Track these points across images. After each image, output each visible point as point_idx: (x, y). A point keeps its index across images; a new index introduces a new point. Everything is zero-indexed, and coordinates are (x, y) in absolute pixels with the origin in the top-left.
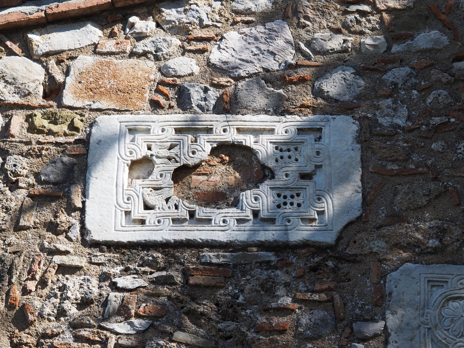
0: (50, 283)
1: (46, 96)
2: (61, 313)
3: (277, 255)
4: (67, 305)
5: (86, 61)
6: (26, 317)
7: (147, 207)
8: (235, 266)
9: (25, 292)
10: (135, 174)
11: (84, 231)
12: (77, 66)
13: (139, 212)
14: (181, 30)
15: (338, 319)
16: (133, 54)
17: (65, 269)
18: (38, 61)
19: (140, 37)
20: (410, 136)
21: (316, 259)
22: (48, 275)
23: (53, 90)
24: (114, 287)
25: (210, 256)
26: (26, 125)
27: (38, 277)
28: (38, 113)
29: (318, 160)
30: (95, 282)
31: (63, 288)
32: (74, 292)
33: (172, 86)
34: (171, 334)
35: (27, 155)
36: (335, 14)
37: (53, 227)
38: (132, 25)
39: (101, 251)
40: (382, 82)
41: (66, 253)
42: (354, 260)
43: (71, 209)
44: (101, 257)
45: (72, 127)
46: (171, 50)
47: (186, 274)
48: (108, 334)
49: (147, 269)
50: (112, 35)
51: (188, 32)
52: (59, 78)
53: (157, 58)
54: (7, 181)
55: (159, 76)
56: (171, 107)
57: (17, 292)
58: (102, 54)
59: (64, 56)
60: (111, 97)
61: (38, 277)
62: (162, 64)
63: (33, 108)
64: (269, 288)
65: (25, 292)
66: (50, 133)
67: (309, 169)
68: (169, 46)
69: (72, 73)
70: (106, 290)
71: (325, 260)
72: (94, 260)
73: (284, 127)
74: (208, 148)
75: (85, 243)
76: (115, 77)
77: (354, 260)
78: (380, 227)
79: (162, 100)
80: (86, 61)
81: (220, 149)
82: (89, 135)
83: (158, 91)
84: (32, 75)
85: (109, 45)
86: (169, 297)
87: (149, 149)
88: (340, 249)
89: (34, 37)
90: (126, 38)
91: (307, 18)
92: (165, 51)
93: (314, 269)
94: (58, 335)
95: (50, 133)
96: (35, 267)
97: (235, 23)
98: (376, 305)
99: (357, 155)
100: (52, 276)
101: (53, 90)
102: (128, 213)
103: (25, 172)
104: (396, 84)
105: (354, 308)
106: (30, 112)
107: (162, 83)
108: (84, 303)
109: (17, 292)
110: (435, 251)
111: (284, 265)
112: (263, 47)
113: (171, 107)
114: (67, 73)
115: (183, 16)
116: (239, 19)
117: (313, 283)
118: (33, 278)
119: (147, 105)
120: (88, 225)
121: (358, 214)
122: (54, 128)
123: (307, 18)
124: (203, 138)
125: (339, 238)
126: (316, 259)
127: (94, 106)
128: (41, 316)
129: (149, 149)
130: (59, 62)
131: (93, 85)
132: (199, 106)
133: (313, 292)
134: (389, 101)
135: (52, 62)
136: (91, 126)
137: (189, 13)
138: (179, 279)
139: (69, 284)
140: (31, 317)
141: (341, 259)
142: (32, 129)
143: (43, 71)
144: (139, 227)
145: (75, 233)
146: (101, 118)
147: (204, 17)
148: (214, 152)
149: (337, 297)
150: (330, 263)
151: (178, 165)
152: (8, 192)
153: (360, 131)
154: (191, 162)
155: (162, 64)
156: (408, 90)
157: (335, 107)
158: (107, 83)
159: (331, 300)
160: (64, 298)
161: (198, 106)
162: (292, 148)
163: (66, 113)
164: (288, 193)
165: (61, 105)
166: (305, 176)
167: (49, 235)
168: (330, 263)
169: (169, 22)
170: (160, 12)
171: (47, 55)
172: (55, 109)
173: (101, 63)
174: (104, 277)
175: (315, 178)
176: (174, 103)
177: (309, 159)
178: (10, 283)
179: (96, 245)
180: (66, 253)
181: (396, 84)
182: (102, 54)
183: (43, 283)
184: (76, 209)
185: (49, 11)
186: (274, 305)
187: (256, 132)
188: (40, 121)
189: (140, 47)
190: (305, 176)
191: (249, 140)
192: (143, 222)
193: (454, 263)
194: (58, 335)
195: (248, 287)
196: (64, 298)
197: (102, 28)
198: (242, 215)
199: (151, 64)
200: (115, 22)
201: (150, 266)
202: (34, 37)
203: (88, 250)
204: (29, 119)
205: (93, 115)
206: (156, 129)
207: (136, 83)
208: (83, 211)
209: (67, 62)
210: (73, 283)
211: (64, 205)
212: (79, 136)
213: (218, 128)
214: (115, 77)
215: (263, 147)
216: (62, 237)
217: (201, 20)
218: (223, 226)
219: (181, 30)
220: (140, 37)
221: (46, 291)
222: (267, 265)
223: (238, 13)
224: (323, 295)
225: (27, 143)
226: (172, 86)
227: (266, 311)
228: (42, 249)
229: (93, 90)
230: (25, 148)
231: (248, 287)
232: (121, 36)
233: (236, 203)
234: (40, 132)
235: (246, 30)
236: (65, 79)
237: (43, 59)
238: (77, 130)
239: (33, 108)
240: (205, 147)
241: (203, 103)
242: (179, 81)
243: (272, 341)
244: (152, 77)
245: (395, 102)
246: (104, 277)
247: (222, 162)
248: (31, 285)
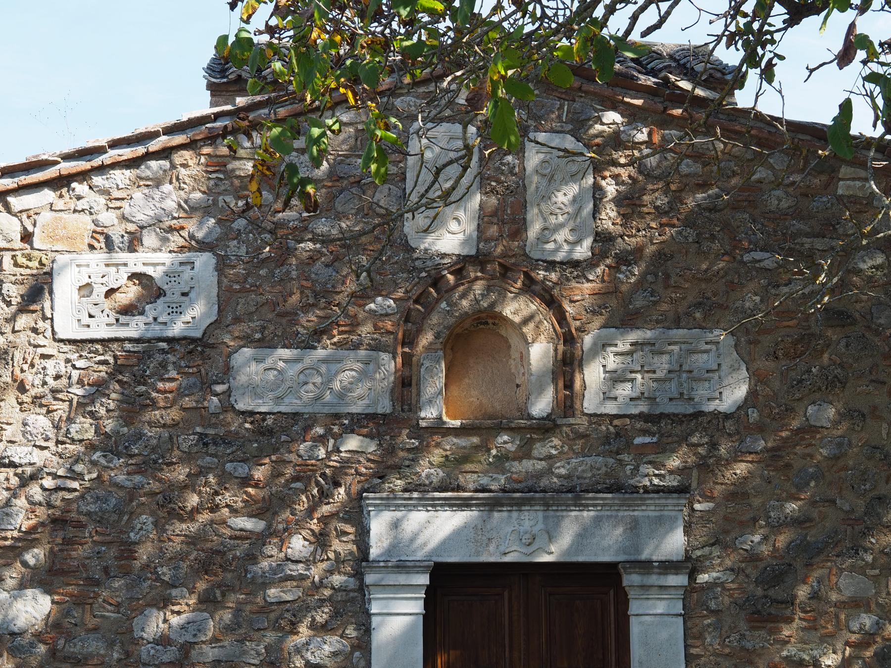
0: (36, 366)
1: (22, 239)
2: (45, 383)
3: (168, 345)
4: (48, 379)
5: (46, 217)
6: (24, 387)
7: (91, 316)
8: (144, 352)
9: (22, 371)
10: (82, 293)
11: (54, 332)
12: (40, 219)
13: (86, 320)
14: (105, 192)
15: (203, 383)
16: (75, 211)
17: (44, 357)
18: (15, 215)
19: (79, 198)
20: (248, 266)
21: (191, 347)
22: (34, 361)
23: (27, 237)
24: (74, 367)
25: (128, 346)
26: (12, 262)
27: (29, 362)
28: (18, 253)
29: (192, 284)
30: (63, 364)
31: (44, 368)
32: (51, 371)
33: (102, 233)
34: (109, 395)
35: (14, 283)
36: (203, 180)
37: (35, 330)
38: (74, 190)
39: (65, 344)
40: (231, 228)
41: (44, 346)
42: (212, 346)
43: (44, 318)
44: (66, 348)
45: (41, 263)
46: (99, 208)
47: (115, 357)
48: (73, 396)
49: (92, 355)
50: (61, 196)
51: (109, 194)
52: (30, 228)
53: (91, 214)
54: (4, 300)
55: (93, 227)
56: (101, 248)
57: (17, 371)
58: (56, 211)
59: (32, 212)
60: (562, 516)
61: (29, 362)
62: (94, 217)
63: (16, 250)
64: (163, 365)
65: (22, 371)
66: (27, 267)
67: (186, 290)
68: (98, 205)
69: (37, 225)
70: (70, 368)
71: (196, 346)
72: (61, 350)
73: (165, 258)
74: (126, 277)
75: (55, 340)
76: (65, 228)
77: (212, 346)
78: (227, 326)
79: (96, 244)
80: (46, 217)
81: (133, 276)
82: (52, 268)
83: (92, 237)
84: (13, 227)
85: (60, 204)
86: (107, 373)
87: (90, 277)
88: (205, 340)
89: (10, 199)
90: (71, 198)
91: (185, 183)
92: (96, 208)
93: (190, 352)
94: (44, 397)
95: (27, 267)
96: (27, 356)
97: (139, 186)
98: (225, 374)
99: (215, 280)
100: (37, 361)
101: (27, 237)
102: (79, 320)
103: (14, 295)
104: (240, 230)
105: (212, 376)
106: (14, 253)
107: (94, 232)
108: (57, 377)
109: (17, 371)
110: (259, 340)
111: (172, 351)
112: (158, 205)
113: (101, 248)
114: (35, 225)
115: (106, 182)
116: (142, 183)
117: (189, 361)
118: (26, 363)
119: (86, 247)
120: (56, 329)
121: (215, 318)
122: (30, 264)
123: (185, 183)
124: (122, 268)
125: (204, 334)
126: (191, 347)
127: (54, 249)
128: (33, 385)
129: (90, 277)
130: (29, 217)
131: (52, 234)
132: (119, 247)
133: (189, 367)
134: (235, 242)
135: (24, 216)
136: (53, 262)
137: (110, 180)
138: (112, 361)
139: (47, 366)
140: (27, 387)
141: (207, 346)
142: (16, 265)
143: (20, 224)
144: (86, 329)
145: (49, 334)
146: (59, 257)
147: (119, 183)
148: (129, 278)
149: (203, 370)
150: (199, 349)
151: (108, 288)
152: (6, 308)
153: (217, 263)
154: (115, 287)
155: (94, 217)
156: (247, 234)
157: (203, 246)
158: (61, 232)
159: (200, 371)
160: (45, 375)
161: (119, 247)
162: (176, 275)
163: (36, 253)
164: (174, 305)
165: (32, 248)
166: (184, 294)
167: (33, 335)
168: (199, 349)
169: (97, 186)
170: (91, 179)
171: (21, 212)
172: (29, 251)
173: (56, 218)
174: (68, 361)
175: (191, 295)
176: (103, 245)
177: (187, 283)
178: (13, 366)
179: (61, 341)
180: (44, 346)
181: (240, 230)
182: (56, 211)
183: (32, 365)
184: (48, 319)
185: (20, 183)
186: (166, 376)
187: (155, 265)
188: (21, 260)
189: (81, 205)
190: (184, 294)
191: (149, 271)
192: (88, 326)
193: (270, 348)
194: (44, 397)
195: (152, 365)
196: (45, 375)
197: (55, 190)
198: (147, 321)
199: (87, 218)
200: (62, 187)
201: (94, 353)
202: (10, 199)
203: (57, 344)
204: (14, 257)
205: (54, 254)
206: (93, 264)
207: (78, 233)
208: (52, 319)
209: (34, 217)
210: (49, 364)
211: (41, 316)
212: (46, 269)
213: (131, 264)
214: (65, 228)
215: (156, 273)
216: (41, 336)
217: (118, 185)
218: (135, 328)
219: (105, 192)
220: (79, 198)
221: (35, 370)
222: (163, 351)
223: (141, 178)
224: (195, 369)
225: (14, 275)
226: (102, 233)
227: (163, 380)
228: (30, 344)
229: (52, 238)
230: (13, 279)
231: (152, 365)
232: (67, 196)
233: (142, 313)
234: (21, 267)
235: (146, 191)
236: (237, 478)
237: (227, 394)
238: (44, 265)
239: (16, 250)
240: (124, 274)
241: (121, 245)
242: (105, 231)
243: (166, 397)
244: (89, 228)
245: (238, 243)
246: (68, 361)
247: (135, 284)
248: (26, 367)
